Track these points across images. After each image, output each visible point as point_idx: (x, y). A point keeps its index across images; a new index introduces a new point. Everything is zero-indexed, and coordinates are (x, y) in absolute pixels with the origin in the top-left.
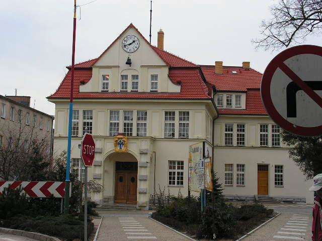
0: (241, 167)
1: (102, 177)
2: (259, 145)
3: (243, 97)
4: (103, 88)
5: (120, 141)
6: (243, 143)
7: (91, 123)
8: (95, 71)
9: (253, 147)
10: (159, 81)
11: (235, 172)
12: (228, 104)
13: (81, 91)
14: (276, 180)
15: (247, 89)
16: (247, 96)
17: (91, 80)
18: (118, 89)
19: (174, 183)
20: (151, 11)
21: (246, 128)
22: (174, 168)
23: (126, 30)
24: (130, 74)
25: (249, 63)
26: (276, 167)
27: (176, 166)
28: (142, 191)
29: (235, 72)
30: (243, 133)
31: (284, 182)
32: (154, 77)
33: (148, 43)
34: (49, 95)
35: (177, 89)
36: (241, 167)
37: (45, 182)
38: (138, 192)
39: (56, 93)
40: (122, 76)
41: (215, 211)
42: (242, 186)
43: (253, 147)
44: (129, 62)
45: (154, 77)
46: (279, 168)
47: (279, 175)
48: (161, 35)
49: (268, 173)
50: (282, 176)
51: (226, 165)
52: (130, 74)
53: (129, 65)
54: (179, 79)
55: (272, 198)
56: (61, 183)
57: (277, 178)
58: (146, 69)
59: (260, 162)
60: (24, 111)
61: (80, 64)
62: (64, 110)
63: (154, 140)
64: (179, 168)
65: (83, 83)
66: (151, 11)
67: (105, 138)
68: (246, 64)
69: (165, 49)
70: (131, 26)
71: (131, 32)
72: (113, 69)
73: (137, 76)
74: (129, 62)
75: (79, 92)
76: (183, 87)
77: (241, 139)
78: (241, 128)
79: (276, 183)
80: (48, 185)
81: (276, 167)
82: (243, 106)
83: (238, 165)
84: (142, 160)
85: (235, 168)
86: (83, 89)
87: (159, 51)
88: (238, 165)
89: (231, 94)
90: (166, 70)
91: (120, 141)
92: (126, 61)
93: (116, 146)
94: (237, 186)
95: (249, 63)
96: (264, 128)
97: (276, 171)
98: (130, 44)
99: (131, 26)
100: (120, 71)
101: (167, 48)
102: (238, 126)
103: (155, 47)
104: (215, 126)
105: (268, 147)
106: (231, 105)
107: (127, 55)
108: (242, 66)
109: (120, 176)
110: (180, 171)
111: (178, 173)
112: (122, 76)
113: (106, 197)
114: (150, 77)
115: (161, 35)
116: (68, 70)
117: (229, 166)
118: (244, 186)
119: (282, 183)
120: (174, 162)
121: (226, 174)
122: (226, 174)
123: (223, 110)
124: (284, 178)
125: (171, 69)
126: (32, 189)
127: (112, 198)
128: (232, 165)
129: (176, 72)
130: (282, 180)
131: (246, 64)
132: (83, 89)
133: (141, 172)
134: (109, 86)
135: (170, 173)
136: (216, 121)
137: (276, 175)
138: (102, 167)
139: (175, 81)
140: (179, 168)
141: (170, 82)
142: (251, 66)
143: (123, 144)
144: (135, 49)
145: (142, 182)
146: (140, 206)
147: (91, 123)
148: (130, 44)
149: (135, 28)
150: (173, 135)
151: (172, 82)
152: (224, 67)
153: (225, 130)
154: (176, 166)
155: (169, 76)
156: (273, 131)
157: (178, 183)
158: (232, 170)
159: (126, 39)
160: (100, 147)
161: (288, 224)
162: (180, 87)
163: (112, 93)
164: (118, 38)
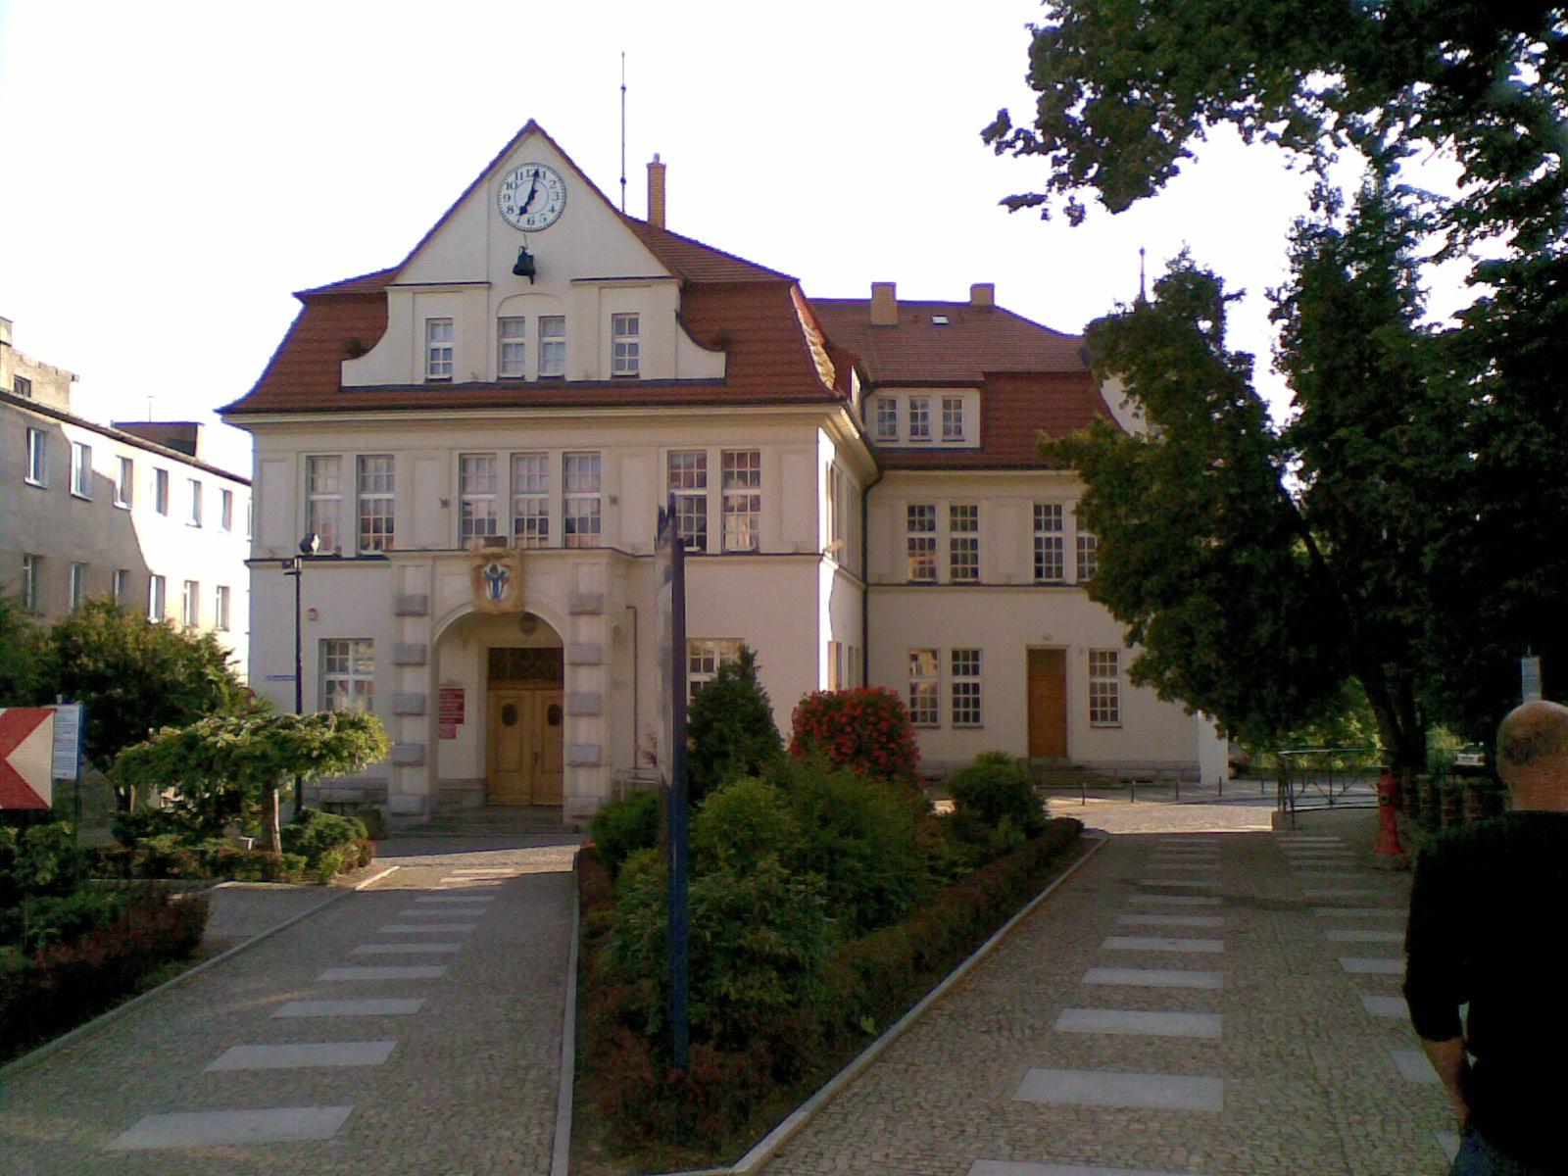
2: (1031, 578)
4: (619, 364)
5: (494, 569)
6: (975, 572)
8: (397, 301)
12: (914, 431)
13: (1276, 785)
14: (1093, 703)
21: (981, 518)
23: (511, 145)
29: (942, 320)
31: (985, 710)
32: (626, 323)
33: (616, 211)
34: (228, 400)
35: (710, 365)
39: (252, 394)
40: (503, 322)
42: (932, 728)
44: (525, 267)
47: (1103, 686)
48: (656, 172)
53: (526, 279)
55: (1079, 768)
57: (1043, 518)
58: (592, 291)
59: (1037, 642)
65: (357, 350)
67: (435, 559)
68: (983, 291)
69: (669, 226)
70: (532, 129)
71: (534, 142)
73: (561, 319)
74: (525, 267)
77: (965, 558)
78: (966, 516)
79: (1093, 716)
82: (972, 438)
84: (579, 636)
86: (355, 373)
87: (652, 233)
89: (925, 391)
91: (494, 569)
92: (515, 261)
93: (478, 581)
96: (1046, 516)
97: (1093, 671)
98: (532, 196)
99: (532, 129)
100: (496, 300)
101: (679, 221)
102: (953, 510)
103: (636, 221)
106: (925, 432)
109: (503, 703)
112: (503, 322)
114: (607, 324)
115: (656, 172)
116: (298, 306)
119: (976, 717)
125: (687, 291)
126: (7, 759)
131: (983, 291)
132: (355, 373)
133: (580, 682)
141: (684, 339)
142: (1001, 300)
143: (506, 581)
144: (551, 217)
148: (532, 196)
149: (544, 133)
151: (694, 339)
152: (901, 302)
155: (681, 318)
159: (511, 179)
163: (465, 386)
164: (483, 176)
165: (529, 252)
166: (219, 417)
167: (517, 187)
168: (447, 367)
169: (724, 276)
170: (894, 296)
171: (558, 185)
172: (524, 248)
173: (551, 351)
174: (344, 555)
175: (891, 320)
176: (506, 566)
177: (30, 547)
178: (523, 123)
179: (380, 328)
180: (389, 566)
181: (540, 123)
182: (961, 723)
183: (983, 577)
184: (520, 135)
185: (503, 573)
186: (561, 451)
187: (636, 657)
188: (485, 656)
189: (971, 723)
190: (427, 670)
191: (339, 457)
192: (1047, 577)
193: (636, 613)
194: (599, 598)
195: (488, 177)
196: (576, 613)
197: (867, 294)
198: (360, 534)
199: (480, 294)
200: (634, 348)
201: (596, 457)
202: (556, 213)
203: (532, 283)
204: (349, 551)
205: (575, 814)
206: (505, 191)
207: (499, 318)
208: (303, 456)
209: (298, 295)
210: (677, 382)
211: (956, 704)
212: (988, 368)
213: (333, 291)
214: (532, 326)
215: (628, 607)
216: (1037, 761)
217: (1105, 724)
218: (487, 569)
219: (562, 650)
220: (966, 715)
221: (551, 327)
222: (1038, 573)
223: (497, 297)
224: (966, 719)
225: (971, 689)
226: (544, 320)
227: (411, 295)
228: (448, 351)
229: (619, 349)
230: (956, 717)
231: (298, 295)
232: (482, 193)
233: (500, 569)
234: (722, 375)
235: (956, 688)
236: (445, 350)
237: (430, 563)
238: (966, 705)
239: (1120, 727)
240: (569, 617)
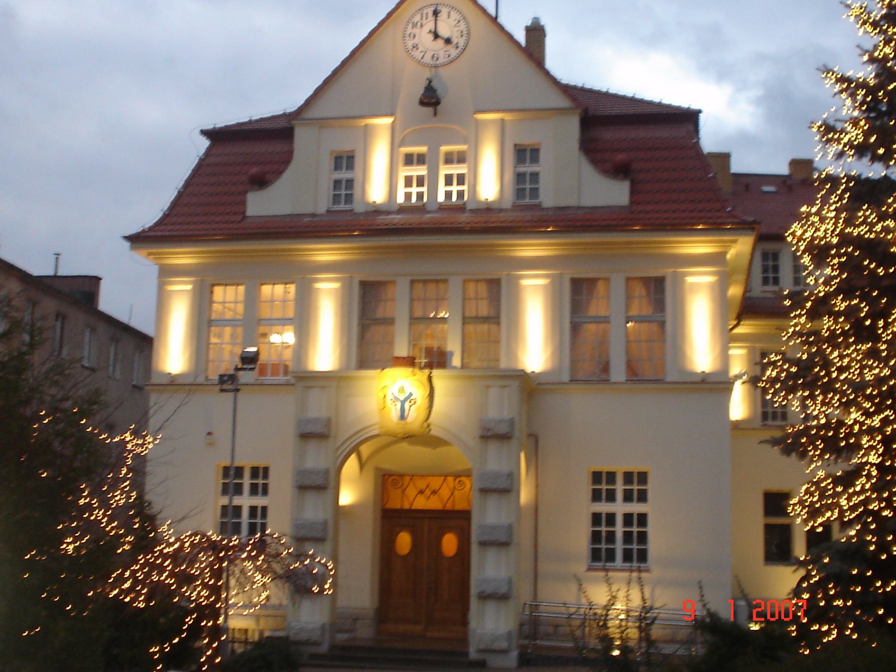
1: (330, 536)
4: (336, 199)
7: (264, 509)
8: (302, 137)
10: (545, 167)
19: (611, 556)
22: (611, 497)
28: (489, 589)
37: (719, 269)
38: (474, 591)
54: (621, 157)
56: (122, 587)
60: (77, 318)
64: (254, 490)
65: (261, 182)
75: (245, 217)
80: (819, 176)
90: (572, 126)
116: (205, 143)
121: (596, 518)
127: (371, 613)
129: (609, 135)
135: (596, 518)
140: (254, 490)
145: (492, 554)
146: (480, 651)
147: (264, 509)
150: (606, 368)
157: (628, 556)
159: (410, 44)
166: (127, 244)
167: (422, 26)
168: (535, 192)
169: (617, 110)
171: (462, 23)
179: (286, 159)
182: (770, 422)
186: (409, 278)
191: (445, 281)
193: (537, 441)
194: (511, 422)
200: (535, 176)
202: (459, 49)
205: (482, 647)
206: (409, 30)
209: (205, 133)
213: (267, 126)
225: (260, 489)
231: (205, 133)
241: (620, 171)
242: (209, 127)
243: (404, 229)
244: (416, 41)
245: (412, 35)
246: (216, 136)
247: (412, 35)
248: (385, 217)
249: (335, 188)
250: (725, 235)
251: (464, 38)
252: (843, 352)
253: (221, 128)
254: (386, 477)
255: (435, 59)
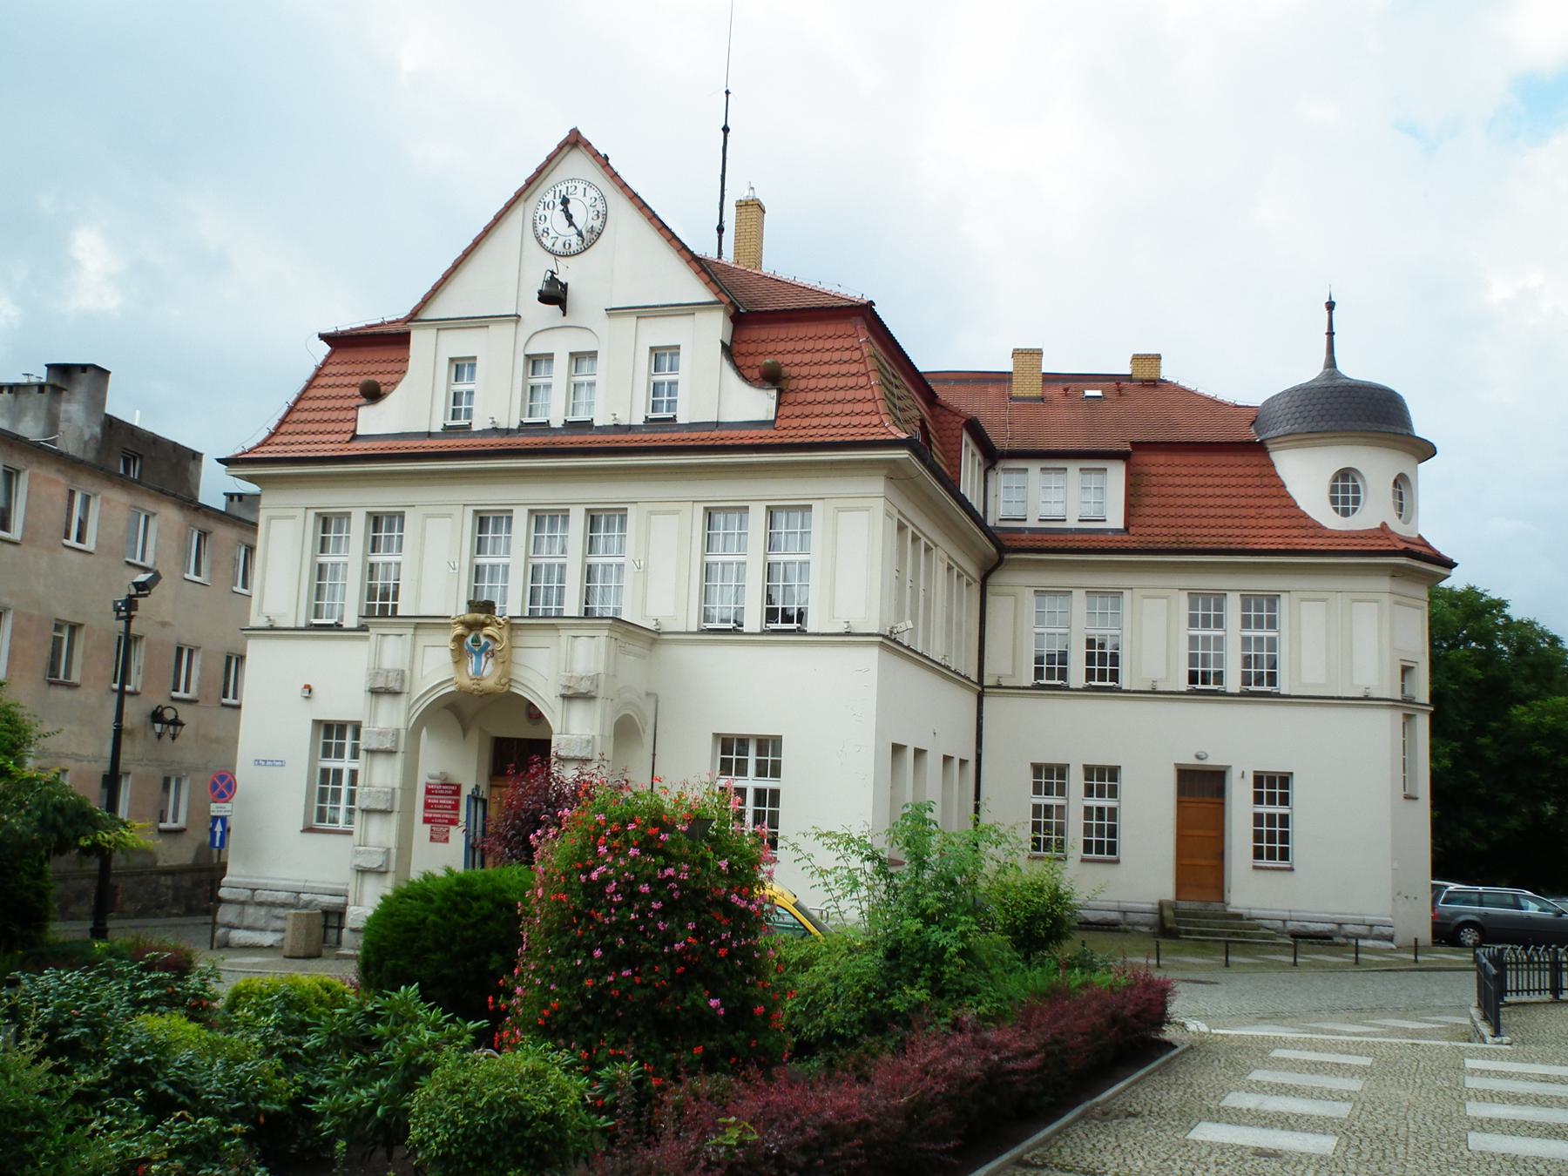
0: (1103, 778)
2: (1184, 685)
3: (1116, 475)
4: (455, 415)
6: (1115, 676)
8: (420, 340)
9: (1154, 693)
10: (684, 376)
11: (1076, 801)
14: (1258, 836)
15: (1132, 443)
16: (1129, 475)
17: (400, 387)
18: (511, 418)
20: (726, 130)
24: (561, 346)
25: (1158, 357)
26: (1259, 779)
27: (752, 758)
30: (1247, 633)
31: (1297, 845)
32: (662, 356)
35: (755, 404)
36: (1103, 778)
41: (569, 1091)
43: (1154, 693)
45: (662, 356)
46: (1273, 786)
48: (752, 209)
49: (1223, 804)
50: (1285, 820)
51: (1037, 769)
52: (561, 346)
55: (1239, 916)
58: (630, 321)
59: (1189, 760)
61: (382, 324)
62: (290, 512)
63: (654, 642)
64: (761, 772)
65: (373, 394)
66: (726, 130)
67: (417, 626)
70: (575, 141)
71: (577, 163)
72: (495, 330)
74: (554, 295)
76: (790, 398)
79: (1258, 854)
81: (1259, 779)
83: (1089, 771)
85: (1076, 782)
86: (375, 421)
88: (1089, 771)
90: (715, 326)
94: (1083, 860)
95: (1158, 357)
97: (1258, 799)
98: (569, 217)
99: (575, 141)
100: (523, 339)
104: (990, 599)
105: (1224, 694)
107: (549, 263)
108: (1128, 371)
110: (767, 783)
111: (760, 794)
113: (200, 920)
114: (644, 358)
117: (1049, 776)
118: (1117, 862)
119: (1285, 855)
120: (743, 742)
121: (1037, 808)
122: (1037, 808)
123: (1026, 535)
124: (1297, 830)
128: (1062, 771)
130: (1285, 837)
132: (375, 421)
134: (477, 407)
136: (993, 580)
137: (1258, 818)
138: (399, 758)
139: (756, 374)
140: (761, 772)
142: (1167, 373)
148: (569, 217)
149: (588, 145)
153: (476, 397)
154: (752, 758)
155: (729, 351)
156: (1246, 623)
158: (1062, 791)
160: (399, 666)
161: (1247, 1101)
162: (774, 393)
163: (484, 433)
164: (518, 196)
165: (561, 278)
168: (672, 405)
170: (1040, 366)
172: (552, 272)
173: (583, 392)
174: (345, 626)
175: (1036, 391)
176: (488, 636)
177: (65, 614)
178: (563, 134)
180: (367, 638)
181: (586, 134)
182: (1265, 863)
183: (1125, 683)
184: (561, 147)
185: (487, 644)
187: (654, 755)
188: (488, 746)
189: (1278, 863)
190: (398, 762)
192: (1202, 683)
194: (594, 679)
195: (525, 196)
196: (569, 698)
197: (1007, 366)
198: (1289, 791)
199: (509, 329)
201: (623, 514)
203: (564, 315)
204: (351, 621)
206: (541, 212)
207: (528, 357)
208: (311, 514)
209: (323, 337)
210: (718, 424)
211: (1088, 830)
212: (1137, 438)
214: (561, 363)
215: (648, 694)
216: (1184, 905)
217: (1271, 863)
218: (469, 640)
219: (550, 741)
220: (1100, 844)
221: (586, 364)
222: (1193, 678)
223: (525, 330)
224: (1100, 851)
226: (576, 357)
227: (435, 331)
228: (470, 393)
229: (656, 388)
230: (1087, 847)
231: (323, 337)
232: (516, 217)
233: (483, 640)
234: (772, 417)
235: (1088, 811)
236: (467, 393)
237: (411, 631)
238: (1048, 826)
239: (1291, 869)
240: (560, 700)
241: (771, 378)
242: (330, 330)
243: (382, 335)
244: (548, 224)
245: (543, 218)
246: (339, 342)
247: (543, 218)
248: (1314, 1036)
249: (1062, 842)
250: (256, 955)
251: (601, 219)
252: (1499, 640)
253: (342, 332)
254: (434, 836)
255: (567, 246)
